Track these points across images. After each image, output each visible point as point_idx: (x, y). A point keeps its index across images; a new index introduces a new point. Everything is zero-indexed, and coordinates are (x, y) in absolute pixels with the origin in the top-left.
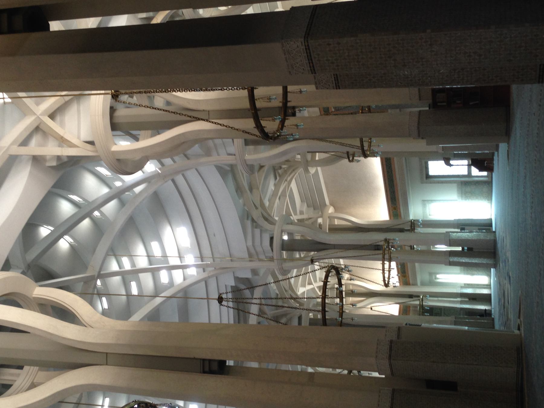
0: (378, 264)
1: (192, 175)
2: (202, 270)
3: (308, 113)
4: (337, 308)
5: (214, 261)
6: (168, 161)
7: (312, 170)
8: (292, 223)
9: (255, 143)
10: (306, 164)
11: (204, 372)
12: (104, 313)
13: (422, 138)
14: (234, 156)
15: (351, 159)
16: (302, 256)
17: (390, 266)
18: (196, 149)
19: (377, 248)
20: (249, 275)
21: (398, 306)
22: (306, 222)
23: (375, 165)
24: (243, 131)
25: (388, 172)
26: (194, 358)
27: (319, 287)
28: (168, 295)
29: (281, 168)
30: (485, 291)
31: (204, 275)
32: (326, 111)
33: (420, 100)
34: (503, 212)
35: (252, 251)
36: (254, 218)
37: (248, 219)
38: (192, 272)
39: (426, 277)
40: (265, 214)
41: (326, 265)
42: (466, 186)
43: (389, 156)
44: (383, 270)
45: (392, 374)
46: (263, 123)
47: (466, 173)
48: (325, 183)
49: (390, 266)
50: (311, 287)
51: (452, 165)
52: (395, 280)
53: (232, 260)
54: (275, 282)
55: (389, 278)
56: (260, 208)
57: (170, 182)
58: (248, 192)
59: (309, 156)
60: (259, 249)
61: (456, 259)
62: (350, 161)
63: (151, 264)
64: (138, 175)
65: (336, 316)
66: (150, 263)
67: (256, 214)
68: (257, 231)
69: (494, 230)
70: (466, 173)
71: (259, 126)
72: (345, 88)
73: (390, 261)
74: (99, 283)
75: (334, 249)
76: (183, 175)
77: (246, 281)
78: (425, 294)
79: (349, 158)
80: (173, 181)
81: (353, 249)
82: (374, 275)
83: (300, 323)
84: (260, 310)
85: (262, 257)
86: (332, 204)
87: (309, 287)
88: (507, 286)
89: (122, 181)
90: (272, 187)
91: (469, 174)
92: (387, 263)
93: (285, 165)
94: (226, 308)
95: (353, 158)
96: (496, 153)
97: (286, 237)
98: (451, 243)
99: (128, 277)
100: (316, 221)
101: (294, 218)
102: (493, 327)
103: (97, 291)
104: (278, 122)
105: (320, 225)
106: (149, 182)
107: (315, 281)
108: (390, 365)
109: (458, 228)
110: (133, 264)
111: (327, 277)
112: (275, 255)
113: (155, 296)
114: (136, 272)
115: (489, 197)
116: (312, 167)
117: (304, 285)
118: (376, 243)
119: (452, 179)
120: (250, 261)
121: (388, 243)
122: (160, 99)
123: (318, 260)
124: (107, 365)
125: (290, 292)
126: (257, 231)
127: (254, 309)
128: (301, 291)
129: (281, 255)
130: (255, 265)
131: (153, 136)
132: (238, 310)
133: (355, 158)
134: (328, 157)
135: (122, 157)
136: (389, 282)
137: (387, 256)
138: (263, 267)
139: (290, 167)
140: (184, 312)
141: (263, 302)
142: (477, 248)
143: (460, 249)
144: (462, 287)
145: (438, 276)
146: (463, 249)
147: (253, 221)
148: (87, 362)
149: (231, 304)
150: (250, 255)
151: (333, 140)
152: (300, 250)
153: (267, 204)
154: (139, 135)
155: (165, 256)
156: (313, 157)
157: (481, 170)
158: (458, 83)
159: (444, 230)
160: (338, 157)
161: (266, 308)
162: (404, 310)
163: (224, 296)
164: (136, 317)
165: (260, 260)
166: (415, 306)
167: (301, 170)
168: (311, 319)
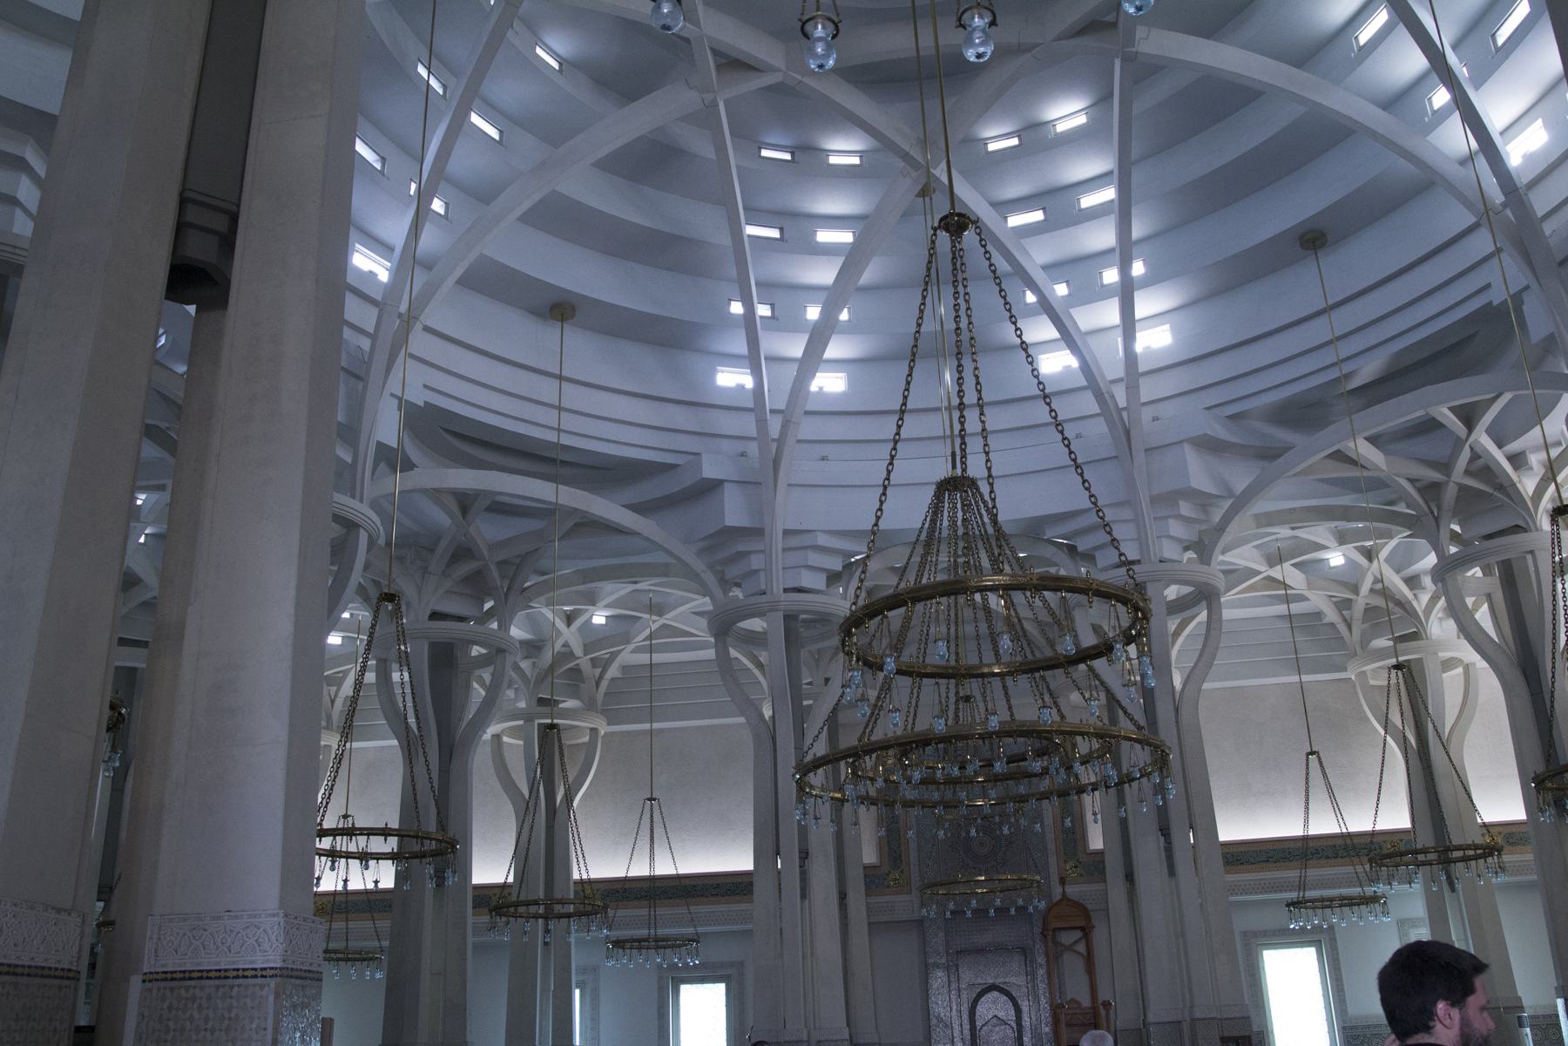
49: (379, 857)
92: (392, 844)
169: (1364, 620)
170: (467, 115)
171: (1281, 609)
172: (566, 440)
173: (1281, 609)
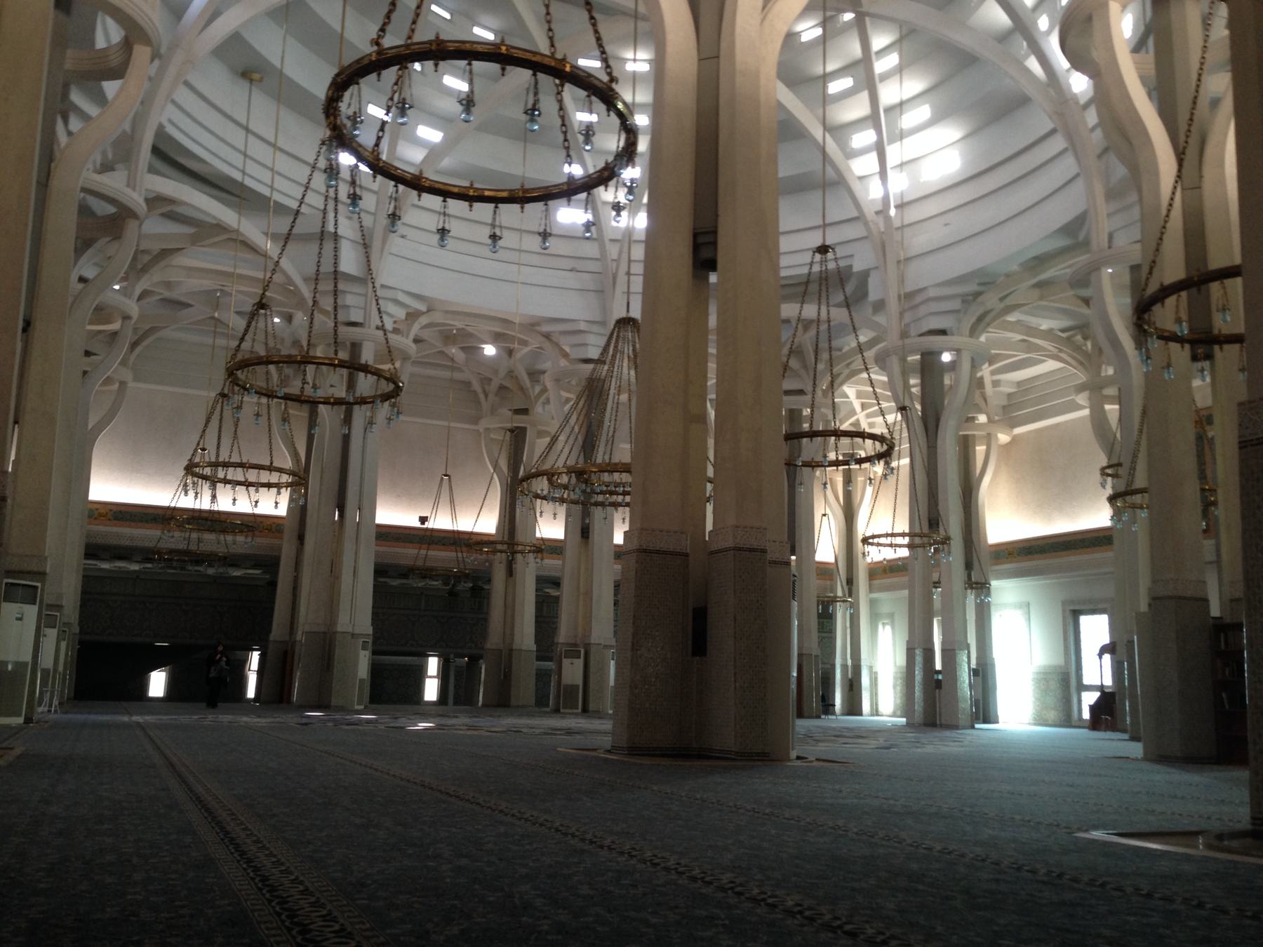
0: (903, 525)
1: (1068, 166)
2: (880, 208)
3: (1201, 386)
4: (819, 458)
5: (898, 229)
6: (1092, 117)
7: (1082, 399)
8: (975, 366)
9: (1137, 286)
10: (1095, 388)
11: (695, 236)
12: (791, 37)
13: (1150, 605)
14: (1106, 245)
15: (1109, 471)
16: (914, 390)
17: (900, 546)
18: (1120, 171)
19: (934, 522)
20: (873, 296)
21: (832, 560)
22: (977, 393)
23: (1099, 517)
24: (1154, 262)
25: (1083, 541)
26: (717, 216)
27: (857, 423)
28: (828, 150)
29: (1085, 338)
30: (866, 706)
31: (869, 211)
32: (1204, 420)
33: (1232, 601)
34: (1008, 743)
35: (918, 299)
36: (981, 297)
37: (979, 284)
38: (874, 192)
39: (885, 609)
40: (988, 319)
41: (896, 436)
42: (1064, 680)
43: (1115, 541)
44: (893, 535)
45: (712, 553)
46: (1171, 301)
47: (1086, 681)
48: (1058, 425)
49: (900, 546)
50: (858, 408)
51: (1100, 658)
52: (876, 555)
53: (899, 262)
54: (859, 345)
55: (879, 545)
56: (1002, 305)
57: (1050, 126)
58: (1034, 281)
59: (1111, 391)
60: (923, 310)
61: (919, 659)
62: (1103, 469)
63: (887, 110)
64: (1061, 62)
65: (805, 456)
66: (889, 110)
67: (991, 300)
68: (956, 304)
69: (977, 726)
70: (1086, 681)
71: (1166, 291)
72: (1243, 461)
73: (910, 546)
74: (848, 16)
75: (929, 447)
76: (1065, 150)
77: (862, 293)
78: (855, 606)
79: (1109, 467)
80: (1053, 132)
81: (929, 483)
82: (885, 517)
83: (787, 393)
84: (811, 321)
85: (908, 317)
86: (1015, 440)
87: (857, 405)
88: (873, 743)
89: (1049, 32)
90: (1045, 325)
91: (1082, 688)
92: (906, 540)
93: (1093, 346)
94: (809, 260)
95: (1108, 475)
96: (1126, 736)
97: (946, 357)
98: (949, 655)
99: (861, 69)
100: (981, 412)
101: (985, 371)
102: (800, 715)
103: (832, 17)
104: (1175, 328)
105: (973, 419)
106: (1048, 85)
107: (868, 416)
108: (727, 550)
109: (978, 664)
110: (885, 77)
111: (873, 437)
112: (912, 341)
113: (827, 128)
114: (869, 83)
115: (1040, 721)
116: (1090, 399)
117: (859, 395)
118: (943, 516)
119: (1073, 657)
120: (899, 296)
121: (943, 543)
122: (1220, 84)
123: (906, 418)
124: (700, 60)
125: (846, 372)
126: (956, 304)
127: (810, 311)
128: (850, 392)
129: (913, 352)
130: (893, 305)
131: (1144, 80)
132: (807, 283)
133: (1109, 479)
134: (1110, 428)
135: (1097, 24)
136: (872, 544)
137: (917, 540)
138: (889, 320)
139: (1085, 354)
140: (800, 186)
141: (824, 327)
142: (943, 696)
143: (938, 666)
144: (871, 668)
145: (888, 628)
146: (939, 672)
147: (977, 295)
148: (702, 20)
149: (816, 268)
150: (909, 296)
151: (1144, 436)
152: (923, 385)
153: (1011, 318)
154: (1147, 52)
155: (902, 135)
156: (1110, 400)
157: (1094, 709)
158: (1251, 672)
159: (972, 639)
160: (1109, 445)
161: (812, 332)
162: (825, 571)
163: (830, 255)
164: (785, 96)
165: (901, 314)
166: (833, 589)
167: (1082, 377)
168: (801, 411)
169: (497, 395)
170: (1103, 408)
171: (446, 374)
172: (249, 182)
173: (446, 374)
